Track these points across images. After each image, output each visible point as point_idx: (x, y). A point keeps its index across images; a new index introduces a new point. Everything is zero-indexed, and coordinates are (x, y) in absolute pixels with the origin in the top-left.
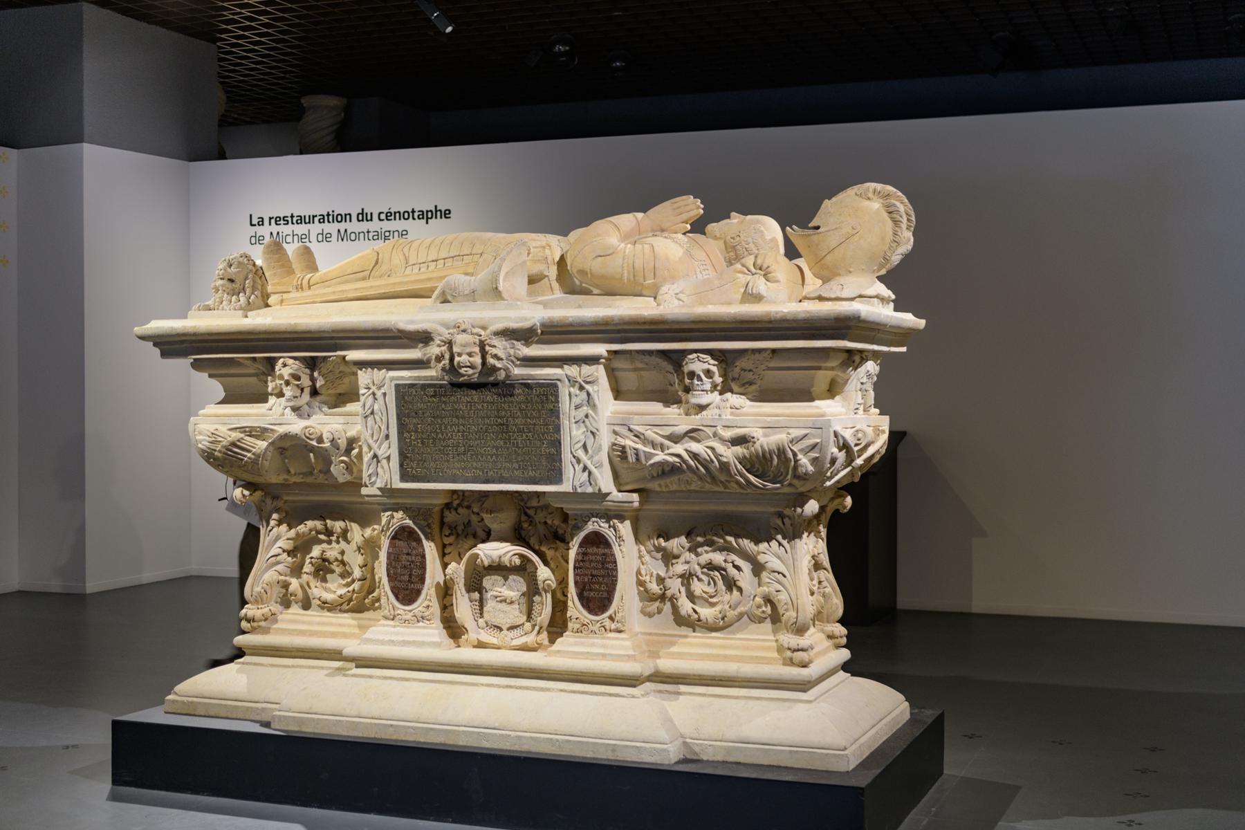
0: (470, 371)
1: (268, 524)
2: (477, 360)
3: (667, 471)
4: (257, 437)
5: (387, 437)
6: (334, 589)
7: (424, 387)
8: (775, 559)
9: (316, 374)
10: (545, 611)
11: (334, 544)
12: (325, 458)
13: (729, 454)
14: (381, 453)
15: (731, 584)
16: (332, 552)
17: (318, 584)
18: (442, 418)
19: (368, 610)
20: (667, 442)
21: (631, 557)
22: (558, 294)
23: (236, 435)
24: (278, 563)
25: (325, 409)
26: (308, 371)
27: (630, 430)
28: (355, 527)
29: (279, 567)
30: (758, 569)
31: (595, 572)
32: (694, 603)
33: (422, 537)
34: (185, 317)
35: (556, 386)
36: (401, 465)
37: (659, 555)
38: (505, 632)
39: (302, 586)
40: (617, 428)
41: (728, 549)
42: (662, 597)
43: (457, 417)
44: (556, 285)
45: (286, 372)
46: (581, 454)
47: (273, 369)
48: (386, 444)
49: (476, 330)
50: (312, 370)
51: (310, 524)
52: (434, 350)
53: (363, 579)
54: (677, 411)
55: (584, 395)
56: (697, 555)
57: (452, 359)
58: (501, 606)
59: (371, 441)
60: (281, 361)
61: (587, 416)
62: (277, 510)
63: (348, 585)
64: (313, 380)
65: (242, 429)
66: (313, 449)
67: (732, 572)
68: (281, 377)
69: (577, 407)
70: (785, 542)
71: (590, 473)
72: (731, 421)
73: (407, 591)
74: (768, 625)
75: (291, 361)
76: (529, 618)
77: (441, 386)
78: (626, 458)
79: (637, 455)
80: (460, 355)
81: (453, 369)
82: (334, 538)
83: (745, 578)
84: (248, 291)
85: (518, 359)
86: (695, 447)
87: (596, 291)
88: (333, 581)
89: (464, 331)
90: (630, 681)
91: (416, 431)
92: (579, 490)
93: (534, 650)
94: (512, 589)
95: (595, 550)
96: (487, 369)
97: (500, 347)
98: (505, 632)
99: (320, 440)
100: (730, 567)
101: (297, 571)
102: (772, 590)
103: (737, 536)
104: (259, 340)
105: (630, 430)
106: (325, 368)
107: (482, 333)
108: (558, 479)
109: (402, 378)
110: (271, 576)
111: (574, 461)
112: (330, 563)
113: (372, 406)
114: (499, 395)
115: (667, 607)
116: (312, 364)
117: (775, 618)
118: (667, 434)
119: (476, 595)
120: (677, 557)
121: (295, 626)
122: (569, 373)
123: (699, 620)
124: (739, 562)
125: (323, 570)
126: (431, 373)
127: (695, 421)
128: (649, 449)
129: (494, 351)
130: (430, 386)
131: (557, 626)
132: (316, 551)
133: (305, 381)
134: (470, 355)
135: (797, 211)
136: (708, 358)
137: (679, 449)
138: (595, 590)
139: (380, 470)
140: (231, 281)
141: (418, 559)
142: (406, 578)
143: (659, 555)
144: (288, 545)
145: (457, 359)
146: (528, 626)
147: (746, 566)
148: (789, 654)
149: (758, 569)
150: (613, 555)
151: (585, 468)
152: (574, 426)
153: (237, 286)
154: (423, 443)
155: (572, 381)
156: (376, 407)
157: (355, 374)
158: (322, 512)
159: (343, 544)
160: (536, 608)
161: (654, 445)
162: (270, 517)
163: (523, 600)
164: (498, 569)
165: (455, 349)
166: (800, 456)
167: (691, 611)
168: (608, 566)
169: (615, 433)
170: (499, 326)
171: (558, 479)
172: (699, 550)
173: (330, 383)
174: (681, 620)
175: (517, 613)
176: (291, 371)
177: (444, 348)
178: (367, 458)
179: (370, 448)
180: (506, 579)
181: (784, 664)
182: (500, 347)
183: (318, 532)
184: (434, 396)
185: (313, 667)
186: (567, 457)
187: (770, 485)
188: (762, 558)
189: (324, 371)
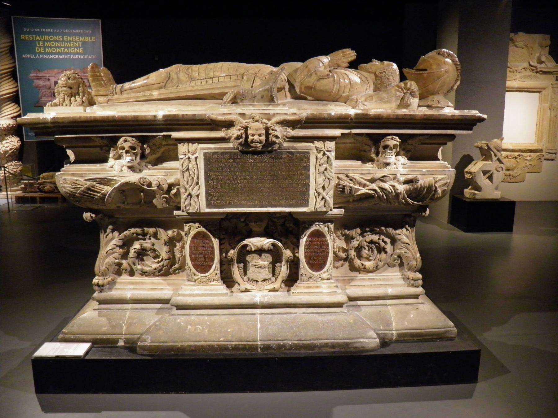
0: (259, 145)
1: (105, 232)
2: (263, 138)
3: (366, 197)
4: (104, 184)
5: (197, 183)
6: (151, 264)
7: (223, 154)
8: (404, 237)
9: (145, 146)
10: (284, 270)
11: (147, 241)
12: (151, 195)
13: (402, 188)
14: (194, 193)
15: (381, 250)
16: (147, 244)
17: (140, 262)
18: (234, 172)
19: (171, 274)
20: (368, 183)
21: (334, 242)
22: (289, 99)
23: (89, 183)
24: (114, 253)
25: (150, 166)
26: (140, 144)
27: (347, 176)
28: (161, 230)
29: (116, 255)
30: (394, 241)
31: (317, 251)
32: (360, 260)
33: (211, 236)
34: (42, 111)
35: (308, 153)
36: (207, 199)
37: (343, 238)
38: (260, 283)
39: (129, 264)
40: (340, 176)
41: (380, 233)
42: (346, 259)
43: (245, 171)
44: (288, 94)
45: (127, 145)
46: (321, 190)
47: (116, 143)
48: (197, 187)
49: (264, 121)
50: (143, 143)
51: (133, 230)
52: (234, 132)
53: (169, 259)
54: (372, 166)
55: (325, 158)
56: (363, 236)
57: (247, 137)
58: (257, 270)
59: (187, 186)
60: (122, 139)
61: (326, 170)
62: (111, 224)
63: (159, 262)
64: (143, 149)
65: (94, 180)
66: (143, 190)
67: (382, 244)
68: (123, 148)
69: (320, 165)
70: (409, 229)
71: (325, 201)
72: (397, 171)
73: (202, 266)
74: (397, 268)
75: (130, 139)
76: (274, 274)
77: (235, 153)
78: (344, 191)
79: (350, 190)
80: (253, 135)
81: (246, 143)
82: (148, 237)
83: (389, 247)
84: (81, 94)
85: (288, 138)
86: (386, 186)
87: (309, 98)
88: (148, 260)
89: (257, 121)
90: (339, 305)
91: (217, 179)
92: (318, 210)
93: (277, 291)
94: (265, 261)
95: (317, 239)
96: (269, 144)
97: (280, 131)
98: (260, 283)
99: (150, 185)
100: (381, 242)
101: (125, 256)
102: (403, 252)
103: (386, 227)
104: (108, 126)
105: (347, 176)
106: (152, 142)
107: (267, 122)
108: (306, 204)
109: (209, 149)
110: (110, 259)
111: (316, 194)
112: (146, 251)
113: (188, 165)
114: (272, 158)
115: (347, 264)
116: (143, 140)
117: (401, 265)
118: (369, 178)
119: (242, 265)
120: (354, 239)
121: (127, 287)
122: (318, 146)
123: (365, 268)
124: (386, 239)
125: (141, 254)
126: (231, 145)
127: (385, 171)
128: (357, 187)
129: (276, 133)
130: (227, 153)
131: (292, 280)
132: (137, 246)
133: (138, 150)
134: (260, 135)
135: (407, 61)
136: (397, 138)
137: (374, 186)
138: (316, 260)
139: (192, 202)
140: (71, 88)
141: (210, 249)
142: (202, 259)
143: (343, 238)
144: (120, 243)
145: (250, 138)
146: (274, 279)
147: (388, 240)
148: (412, 282)
149: (394, 241)
150: (327, 241)
151: (323, 198)
152: (318, 175)
153: (74, 90)
154: (221, 186)
155: (318, 150)
156: (190, 166)
157: (176, 145)
158: (142, 223)
159: (153, 240)
160: (277, 269)
161: (360, 184)
162: (107, 227)
163: (271, 266)
164: (260, 251)
165: (249, 132)
166: (438, 189)
167: (361, 265)
168: (324, 247)
169: (338, 178)
170: (281, 118)
171: (306, 204)
172: (365, 234)
173: (152, 152)
174: (353, 268)
175: (267, 273)
176: (130, 145)
177: (243, 131)
178: (183, 196)
179: (186, 189)
180: (260, 255)
181: (408, 287)
182: (280, 131)
183: (139, 235)
184: (229, 159)
185: (143, 309)
186: (312, 192)
187: (416, 203)
188: (398, 237)
189: (151, 144)
